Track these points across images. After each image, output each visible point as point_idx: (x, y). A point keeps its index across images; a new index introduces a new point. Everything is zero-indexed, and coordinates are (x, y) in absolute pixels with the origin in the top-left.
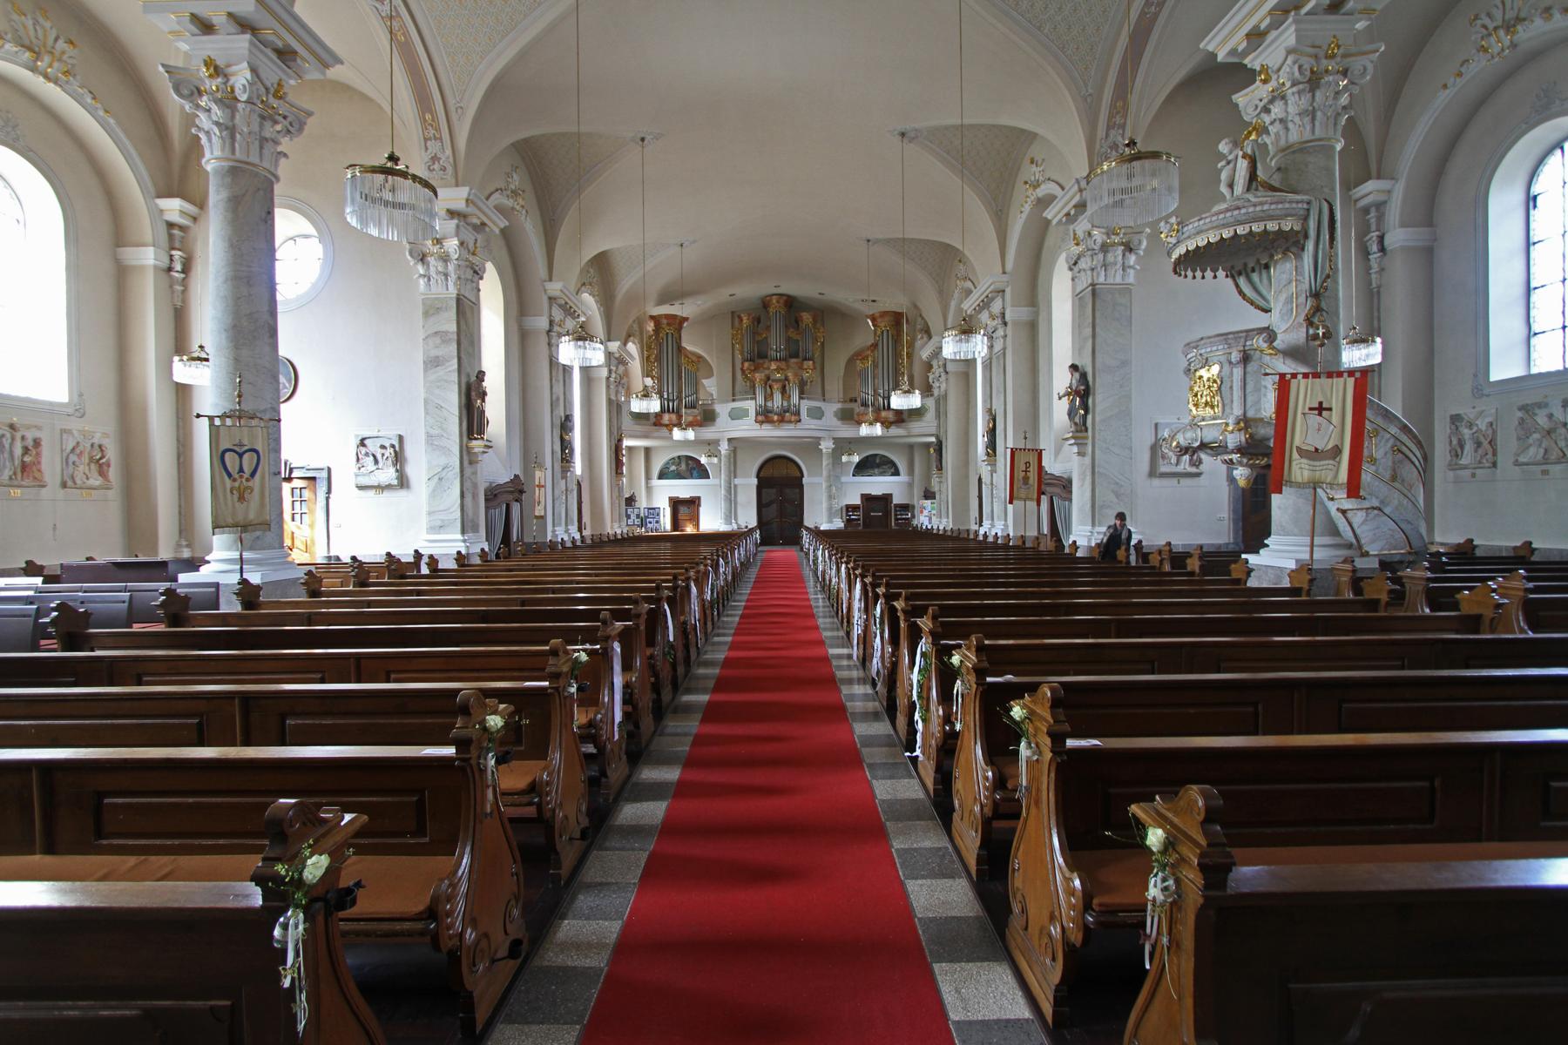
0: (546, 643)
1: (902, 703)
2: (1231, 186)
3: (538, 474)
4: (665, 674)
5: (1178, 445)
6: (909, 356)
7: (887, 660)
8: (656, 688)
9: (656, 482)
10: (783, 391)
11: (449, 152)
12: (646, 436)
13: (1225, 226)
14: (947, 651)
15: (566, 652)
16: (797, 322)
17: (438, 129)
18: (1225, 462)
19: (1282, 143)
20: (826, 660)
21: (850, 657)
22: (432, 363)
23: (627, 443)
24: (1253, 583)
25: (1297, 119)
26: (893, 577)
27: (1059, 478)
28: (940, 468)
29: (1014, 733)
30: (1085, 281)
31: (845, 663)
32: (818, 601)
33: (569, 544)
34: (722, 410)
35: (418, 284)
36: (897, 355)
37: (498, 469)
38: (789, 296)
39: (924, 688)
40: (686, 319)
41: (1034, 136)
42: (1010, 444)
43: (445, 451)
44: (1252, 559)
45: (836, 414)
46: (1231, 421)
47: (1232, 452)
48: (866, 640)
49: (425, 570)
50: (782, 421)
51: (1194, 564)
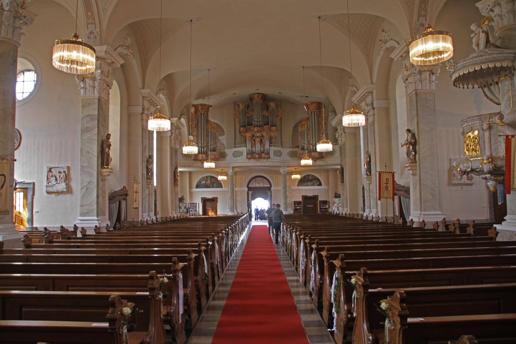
0: (148, 273)
1: (325, 304)
2: (478, 45)
3: (135, 186)
4: (203, 290)
5: (461, 170)
6: (326, 124)
7: (318, 282)
8: (199, 298)
9: (195, 190)
10: (261, 142)
11: (98, 29)
12: (189, 166)
13: (476, 64)
14: (349, 276)
15: (157, 278)
16: (267, 107)
17: (94, 19)
18: (483, 178)
19: (500, 26)
20: (285, 282)
21: (298, 281)
22: (85, 130)
23: (179, 169)
24: (499, 239)
25: (507, 15)
26: (320, 239)
27: (403, 187)
28: (343, 182)
29: (383, 316)
30: (411, 88)
31: (295, 284)
32: (281, 251)
33: (176, 218)
34: (229, 152)
35: (81, 91)
36: (319, 124)
37: (115, 184)
38: (263, 94)
39: (337, 296)
40: (211, 106)
41: (384, 19)
42: (378, 170)
43: (90, 174)
44: (498, 227)
45: (288, 154)
46: (485, 158)
47: (486, 173)
48: (306, 272)
49: (79, 235)
50: (260, 157)
51: (470, 230)
